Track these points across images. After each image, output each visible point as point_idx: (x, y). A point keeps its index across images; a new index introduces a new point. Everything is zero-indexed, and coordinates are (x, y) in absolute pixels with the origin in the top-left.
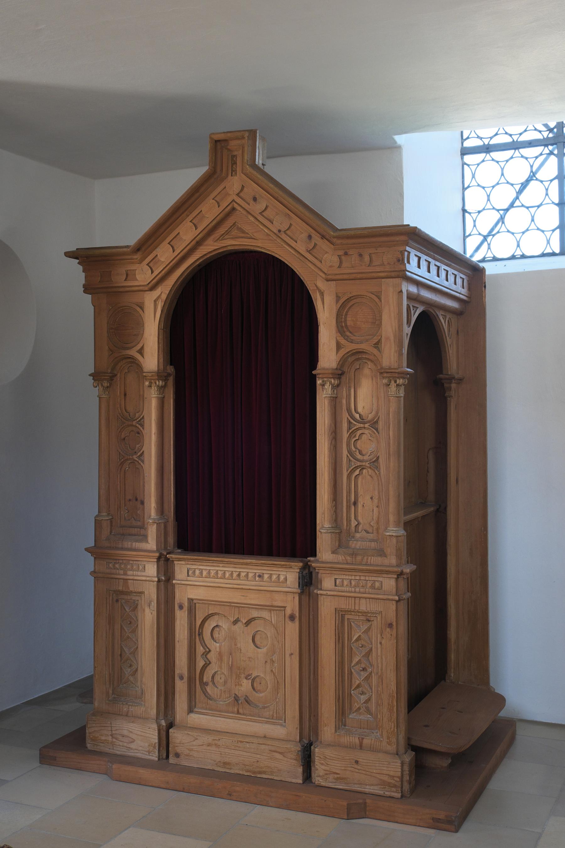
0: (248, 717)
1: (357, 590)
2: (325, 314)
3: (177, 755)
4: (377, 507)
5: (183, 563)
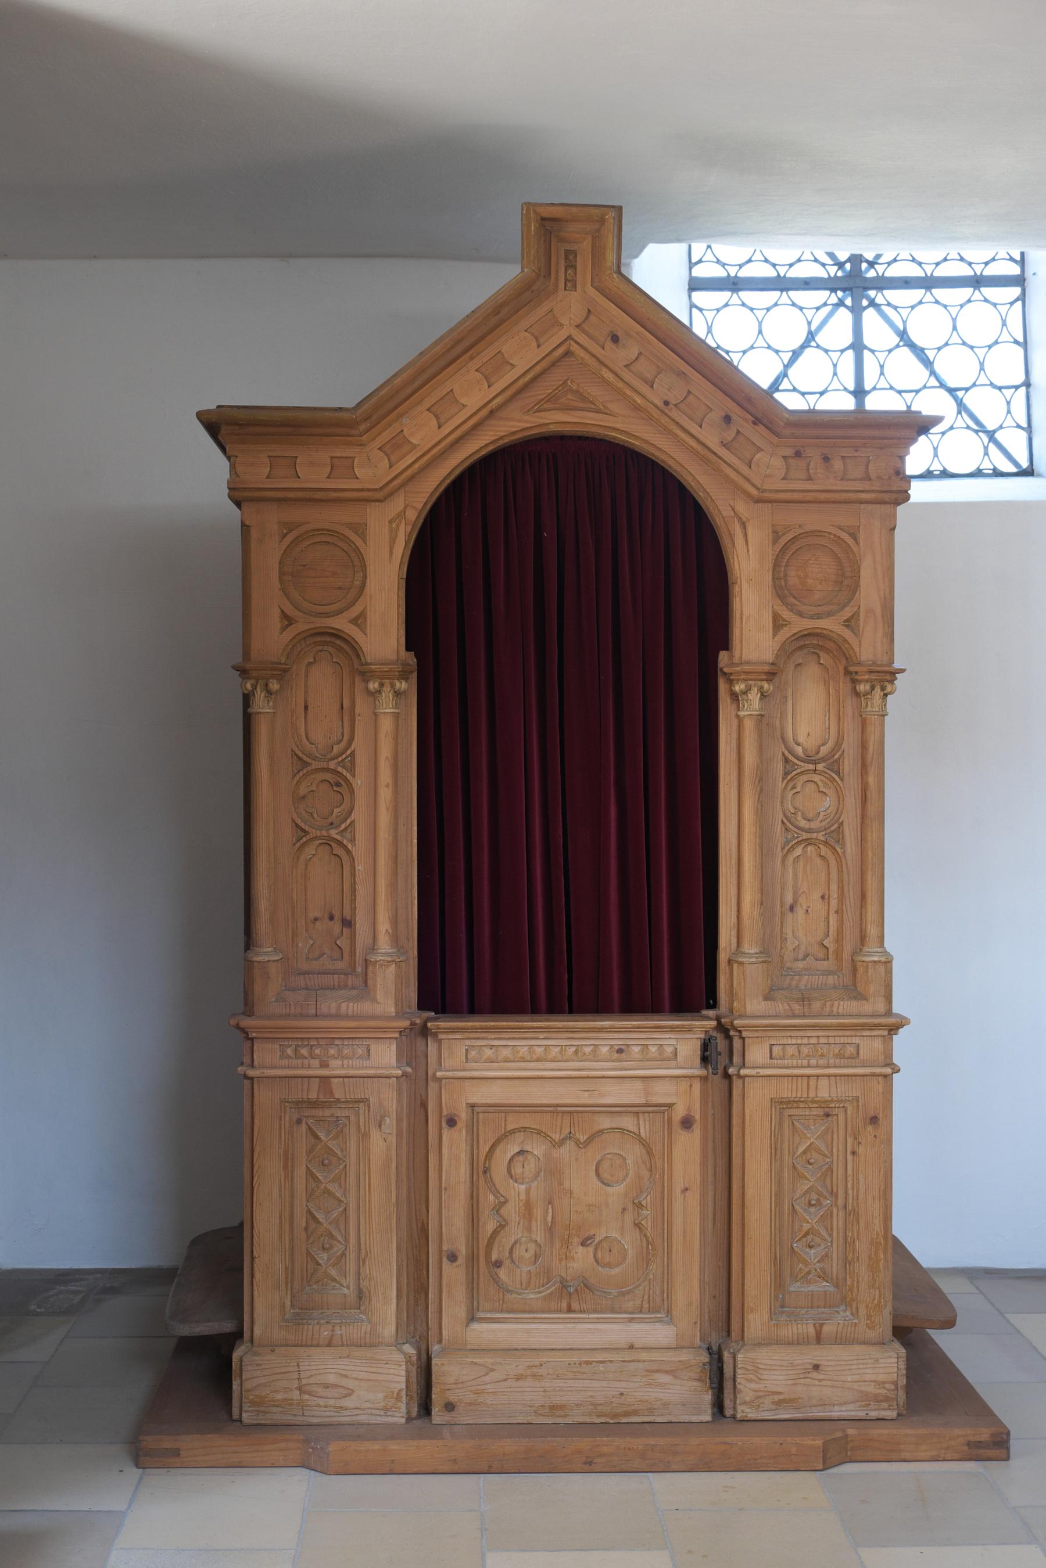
0: (591, 1316)
1: (813, 1062)
2: (748, 563)
3: (450, 1407)
4: (837, 912)
5: (458, 1036)
